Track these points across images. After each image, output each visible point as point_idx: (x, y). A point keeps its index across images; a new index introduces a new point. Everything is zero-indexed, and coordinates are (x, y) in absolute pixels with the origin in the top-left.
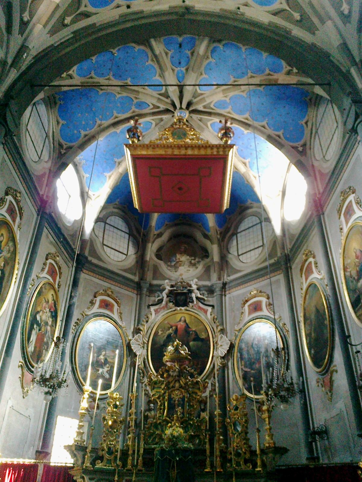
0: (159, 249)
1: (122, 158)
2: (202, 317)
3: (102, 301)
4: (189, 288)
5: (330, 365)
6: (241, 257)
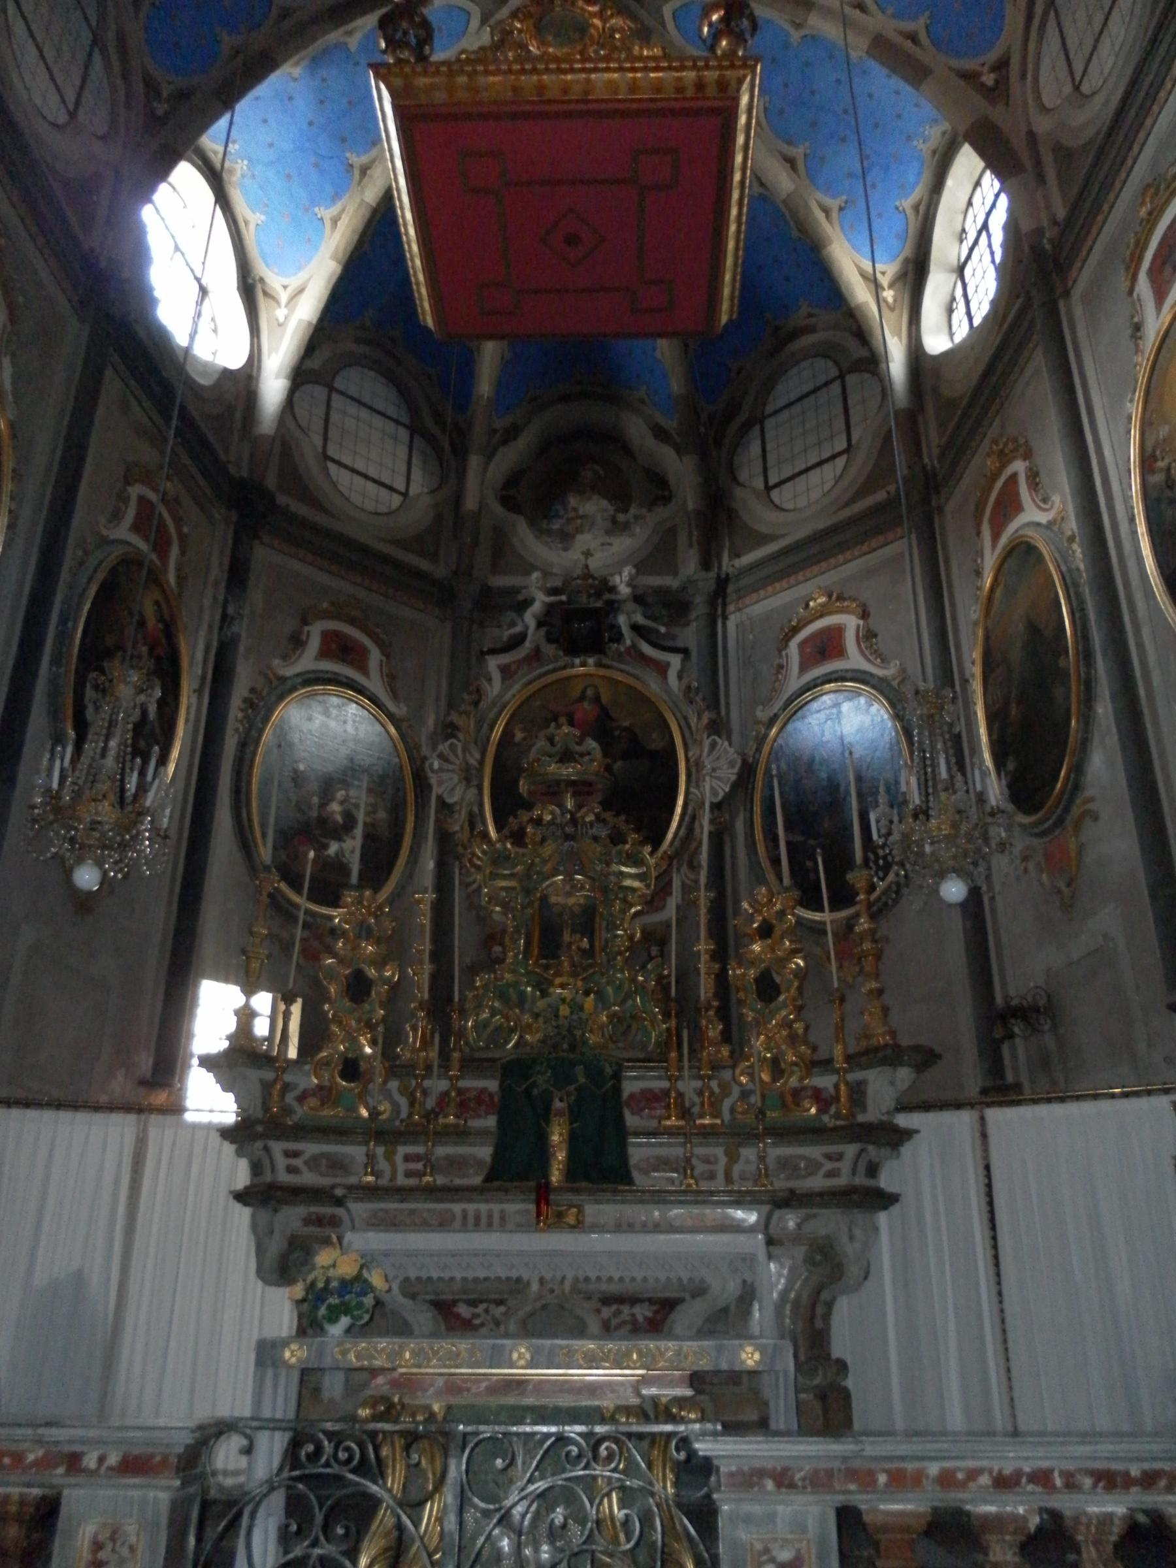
0: (513, 480)
1: (374, 152)
2: (652, 685)
3: (327, 636)
4: (607, 596)
5: (1071, 801)
6: (775, 494)
